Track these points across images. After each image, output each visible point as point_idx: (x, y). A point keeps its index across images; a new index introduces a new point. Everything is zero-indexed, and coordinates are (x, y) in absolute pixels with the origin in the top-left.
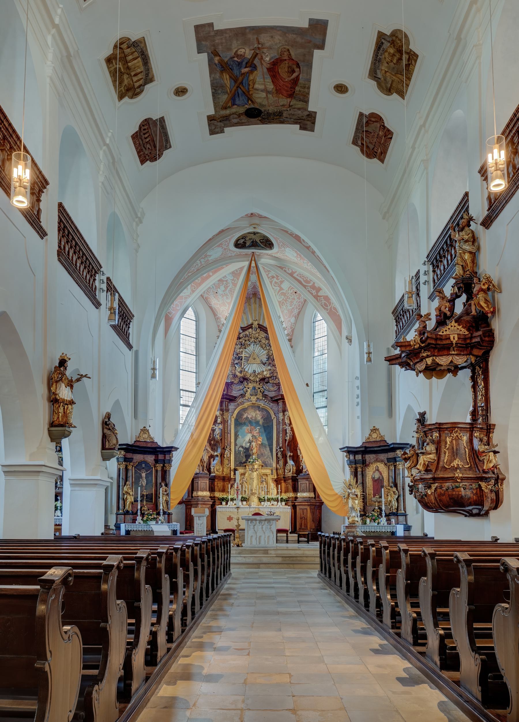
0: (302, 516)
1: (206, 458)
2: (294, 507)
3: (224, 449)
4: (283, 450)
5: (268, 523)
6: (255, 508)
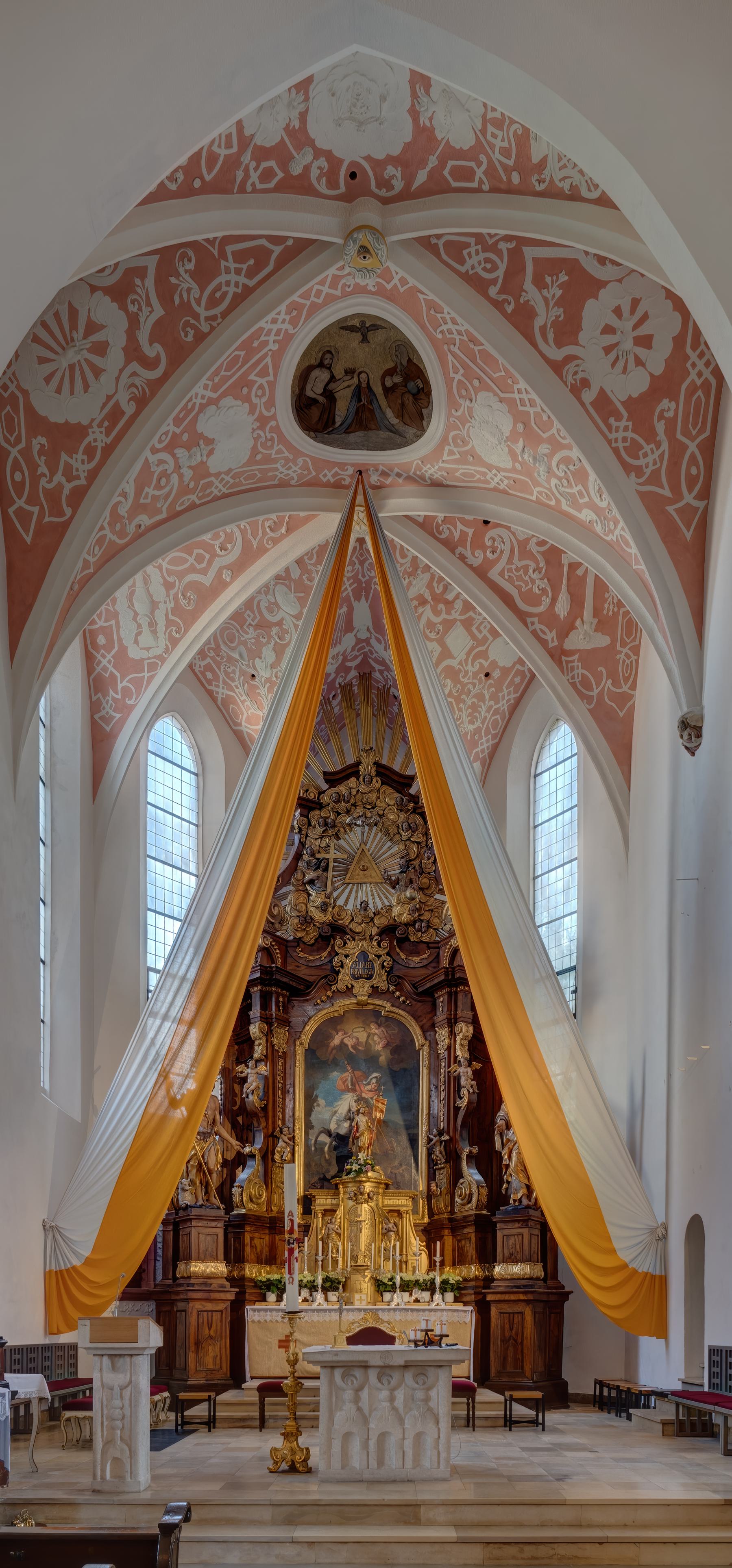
0: (507, 1334)
1: (214, 1161)
2: (482, 1308)
3: (272, 1138)
4: (448, 1138)
5: (415, 1376)
6: (365, 1310)
